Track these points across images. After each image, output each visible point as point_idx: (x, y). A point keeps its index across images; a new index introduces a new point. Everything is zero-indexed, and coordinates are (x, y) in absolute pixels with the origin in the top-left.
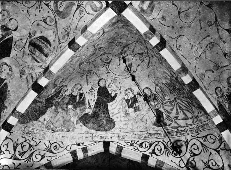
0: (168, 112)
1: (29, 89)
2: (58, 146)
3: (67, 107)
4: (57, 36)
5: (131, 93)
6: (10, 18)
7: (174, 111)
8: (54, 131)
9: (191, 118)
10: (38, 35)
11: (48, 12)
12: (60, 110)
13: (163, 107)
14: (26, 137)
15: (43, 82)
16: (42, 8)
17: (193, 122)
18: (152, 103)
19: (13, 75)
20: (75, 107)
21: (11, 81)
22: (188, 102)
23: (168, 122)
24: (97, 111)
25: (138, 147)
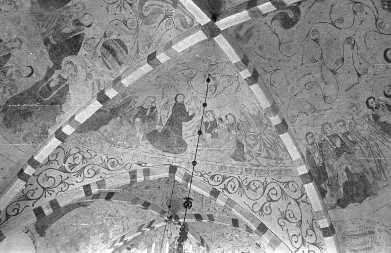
0: (250, 146)
1: (93, 97)
2: (116, 162)
3: (134, 120)
4: (136, 44)
5: (211, 115)
6: (86, 12)
7: (258, 145)
8: (114, 144)
9: (274, 159)
10: (114, 37)
11: (131, 13)
12: (125, 122)
13: (245, 139)
14: (80, 147)
15: (111, 93)
16: (124, 7)
17: (276, 163)
18: (233, 132)
19: (77, 77)
20: (143, 122)
21: (73, 83)
22: (274, 141)
23: (248, 157)
24: (168, 129)
25: (209, 179)
